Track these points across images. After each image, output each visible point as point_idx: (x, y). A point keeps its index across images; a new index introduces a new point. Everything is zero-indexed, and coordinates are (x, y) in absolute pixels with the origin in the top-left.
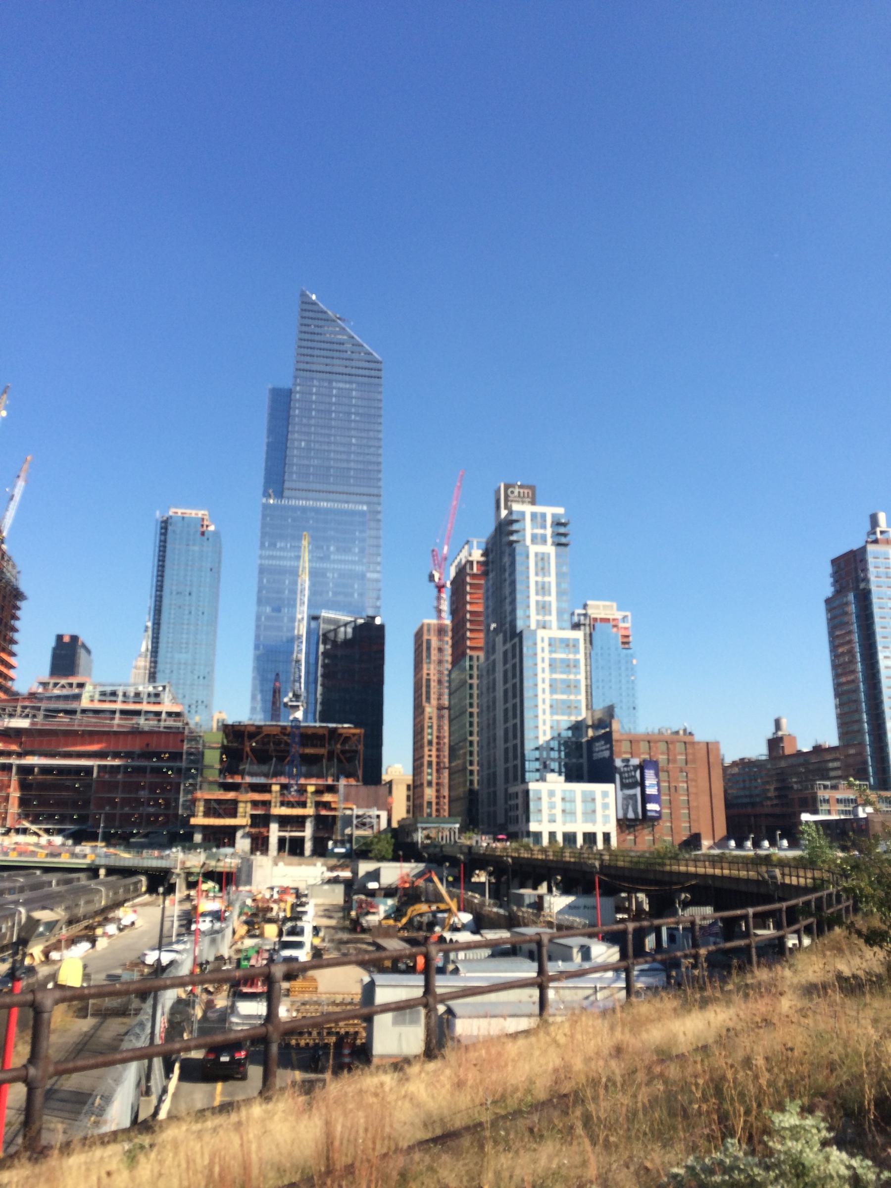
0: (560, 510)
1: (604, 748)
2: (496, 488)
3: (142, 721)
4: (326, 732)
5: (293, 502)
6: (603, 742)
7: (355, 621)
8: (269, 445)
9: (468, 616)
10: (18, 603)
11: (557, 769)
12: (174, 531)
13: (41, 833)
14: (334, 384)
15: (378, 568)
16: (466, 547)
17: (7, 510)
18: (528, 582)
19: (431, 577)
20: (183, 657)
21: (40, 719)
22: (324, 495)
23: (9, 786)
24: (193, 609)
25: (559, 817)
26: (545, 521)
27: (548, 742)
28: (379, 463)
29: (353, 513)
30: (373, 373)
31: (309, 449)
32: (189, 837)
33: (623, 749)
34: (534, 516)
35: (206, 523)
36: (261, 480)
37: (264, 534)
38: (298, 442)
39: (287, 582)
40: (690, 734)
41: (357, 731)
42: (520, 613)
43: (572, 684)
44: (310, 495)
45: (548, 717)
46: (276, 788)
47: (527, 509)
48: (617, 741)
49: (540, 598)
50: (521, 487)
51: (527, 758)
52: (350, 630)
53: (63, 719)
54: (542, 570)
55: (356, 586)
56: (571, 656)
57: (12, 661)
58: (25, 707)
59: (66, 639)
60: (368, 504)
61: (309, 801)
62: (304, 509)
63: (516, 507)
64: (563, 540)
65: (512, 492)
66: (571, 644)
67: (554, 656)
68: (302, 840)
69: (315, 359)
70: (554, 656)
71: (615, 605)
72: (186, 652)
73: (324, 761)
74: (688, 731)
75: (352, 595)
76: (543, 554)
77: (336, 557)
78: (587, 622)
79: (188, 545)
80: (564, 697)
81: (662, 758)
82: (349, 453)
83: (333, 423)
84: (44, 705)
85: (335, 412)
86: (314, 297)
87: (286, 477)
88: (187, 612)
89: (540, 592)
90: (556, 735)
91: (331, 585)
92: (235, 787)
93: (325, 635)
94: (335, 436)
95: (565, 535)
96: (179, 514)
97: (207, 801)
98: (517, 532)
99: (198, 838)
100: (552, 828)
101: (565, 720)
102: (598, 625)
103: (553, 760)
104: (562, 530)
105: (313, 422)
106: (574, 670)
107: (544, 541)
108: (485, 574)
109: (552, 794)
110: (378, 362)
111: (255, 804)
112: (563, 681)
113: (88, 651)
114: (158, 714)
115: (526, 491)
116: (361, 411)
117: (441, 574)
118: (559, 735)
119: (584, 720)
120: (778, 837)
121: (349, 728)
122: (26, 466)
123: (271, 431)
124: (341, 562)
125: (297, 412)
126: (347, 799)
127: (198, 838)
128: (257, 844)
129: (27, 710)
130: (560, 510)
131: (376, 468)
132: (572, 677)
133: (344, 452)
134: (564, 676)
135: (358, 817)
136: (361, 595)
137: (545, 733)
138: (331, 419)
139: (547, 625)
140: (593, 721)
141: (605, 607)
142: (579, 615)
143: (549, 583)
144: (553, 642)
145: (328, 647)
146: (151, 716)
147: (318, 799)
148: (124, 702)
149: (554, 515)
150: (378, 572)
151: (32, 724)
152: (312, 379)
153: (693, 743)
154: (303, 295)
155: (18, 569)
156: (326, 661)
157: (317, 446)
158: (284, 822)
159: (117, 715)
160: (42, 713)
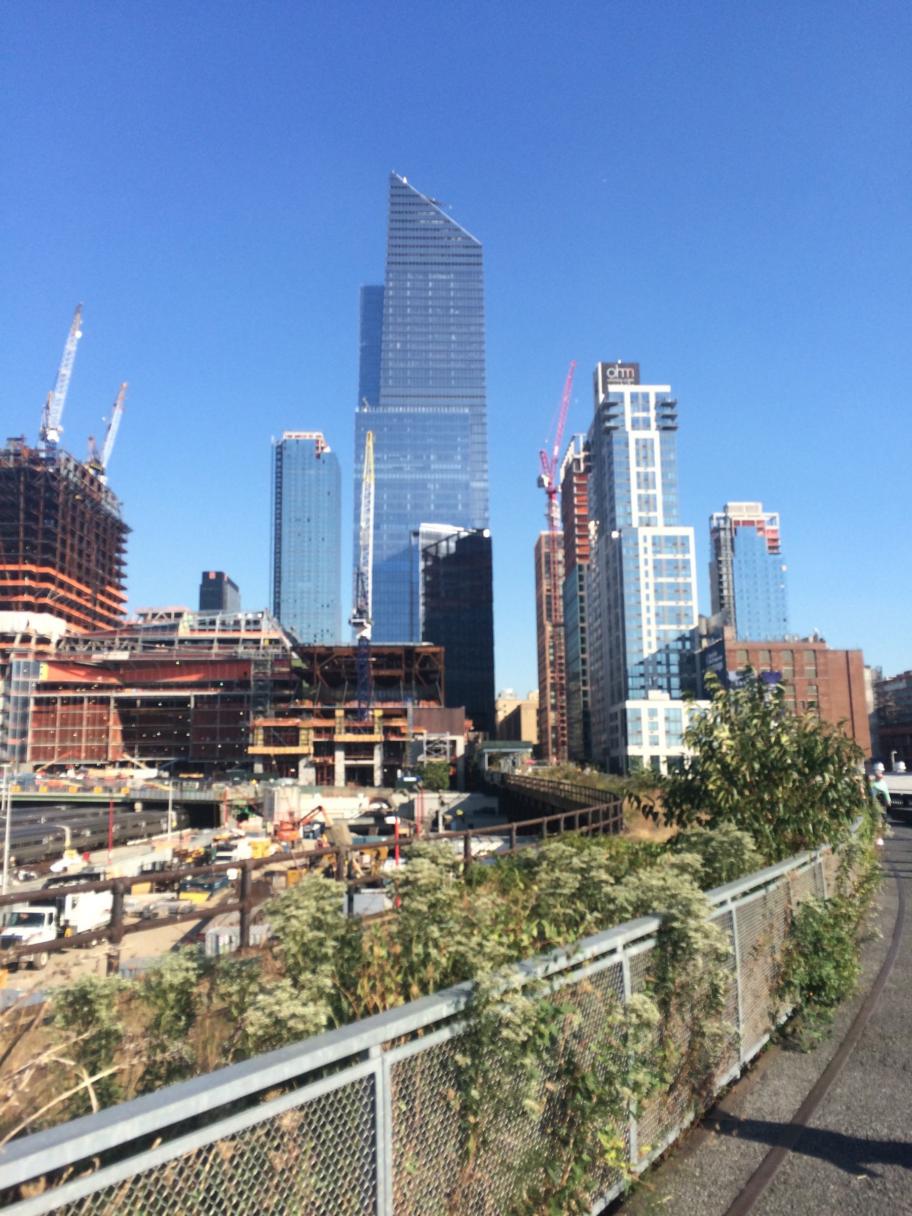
0: (666, 389)
1: (716, 659)
2: (593, 370)
3: (240, 649)
4: (402, 652)
5: (391, 410)
6: (715, 654)
7: (458, 534)
8: (363, 350)
9: (576, 521)
10: (124, 536)
11: (665, 685)
12: (289, 456)
13: (142, 765)
14: (430, 276)
15: (485, 477)
16: (572, 444)
17: (105, 440)
18: (628, 474)
19: (540, 482)
20: (306, 585)
21: (138, 651)
22: (423, 400)
23: (108, 720)
24: (313, 536)
25: (663, 739)
26: (648, 402)
27: (654, 656)
28: (482, 361)
29: (452, 417)
30: (472, 260)
31: (404, 351)
32: (249, 766)
33: (738, 660)
34: (634, 397)
35: (320, 445)
36: (357, 389)
38: (393, 343)
39: (385, 496)
40: (822, 641)
41: (437, 649)
42: (619, 510)
43: (682, 589)
44: (409, 400)
45: (653, 627)
46: (339, 713)
47: (627, 390)
48: (730, 651)
49: (642, 492)
50: (621, 366)
51: (630, 674)
52: (452, 545)
53: (162, 650)
54: (645, 457)
55: (460, 497)
56: (680, 557)
57: (122, 594)
58: (122, 640)
59: (212, 576)
60: (471, 406)
61: (376, 726)
62: (400, 417)
63: (612, 388)
64: (669, 423)
65: (612, 373)
66: (679, 542)
67: (659, 556)
68: (371, 768)
69: (408, 250)
70: (659, 556)
71: (760, 505)
72: (309, 580)
73: (401, 684)
74: (820, 637)
75: (456, 506)
76: (646, 440)
78: (728, 526)
79: (304, 469)
80: (672, 603)
81: (786, 670)
82: (448, 352)
83: (431, 320)
84: (141, 637)
86: (405, 181)
87: (382, 381)
88: (306, 539)
89: (643, 484)
90: (663, 647)
91: (432, 497)
92: (296, 713)
93: (425, 551)
94: (432, 333)
95: (672, 417)
97: (266, 729)
98: (614, 417)
99: (259, 768)
100: (655, 751)
101: (673, 630)
102: (740, 528)
103: (661, 675)
104: (668, 411)
105: (408, 320)
106: (683, 572)
107: (647, 426)
108: (588, 469)
109: (653, 713)
110: (479, 247)
111: (318, 731)
112: (670, 585)
113: (236, 588)
114: (257, 641)
115: (628, 370)
116: (460, 303)
117: (551, 478)
118: (667, 647)
119: (697, 628)
120: (893, 759)
122: (122, 394)
123: (365, 334)
124: (442, 471)
125: (391, 310)
126: (417, 723)
127: (259, 768)
128: (322, 774)
129: (125, 643)
130: (666, 389)
131: (478, 366)
132: (681, 580)
134: (671, 580)
135: (428, 742)
136: (466, 506)
137: (650, 646)
138: (428, 315)
139: (652, 522)
140: (708, 630)
141: (748, 508)
142: (718, 519)
143: (654, 473)
144: (657, 541)
145: (429, 563)
146: (250, 644)
147: (386, 724)
148: (224, 631)
149: (658, 395)
150: (485, 481)
151: (131, 656)
152: (405, 273)
153: (825, 652)
154: (393, 178)
155: (120, 500)
156: (428, 579)
158: (351, 749)
159: (216, 644)
160: (140, 644)
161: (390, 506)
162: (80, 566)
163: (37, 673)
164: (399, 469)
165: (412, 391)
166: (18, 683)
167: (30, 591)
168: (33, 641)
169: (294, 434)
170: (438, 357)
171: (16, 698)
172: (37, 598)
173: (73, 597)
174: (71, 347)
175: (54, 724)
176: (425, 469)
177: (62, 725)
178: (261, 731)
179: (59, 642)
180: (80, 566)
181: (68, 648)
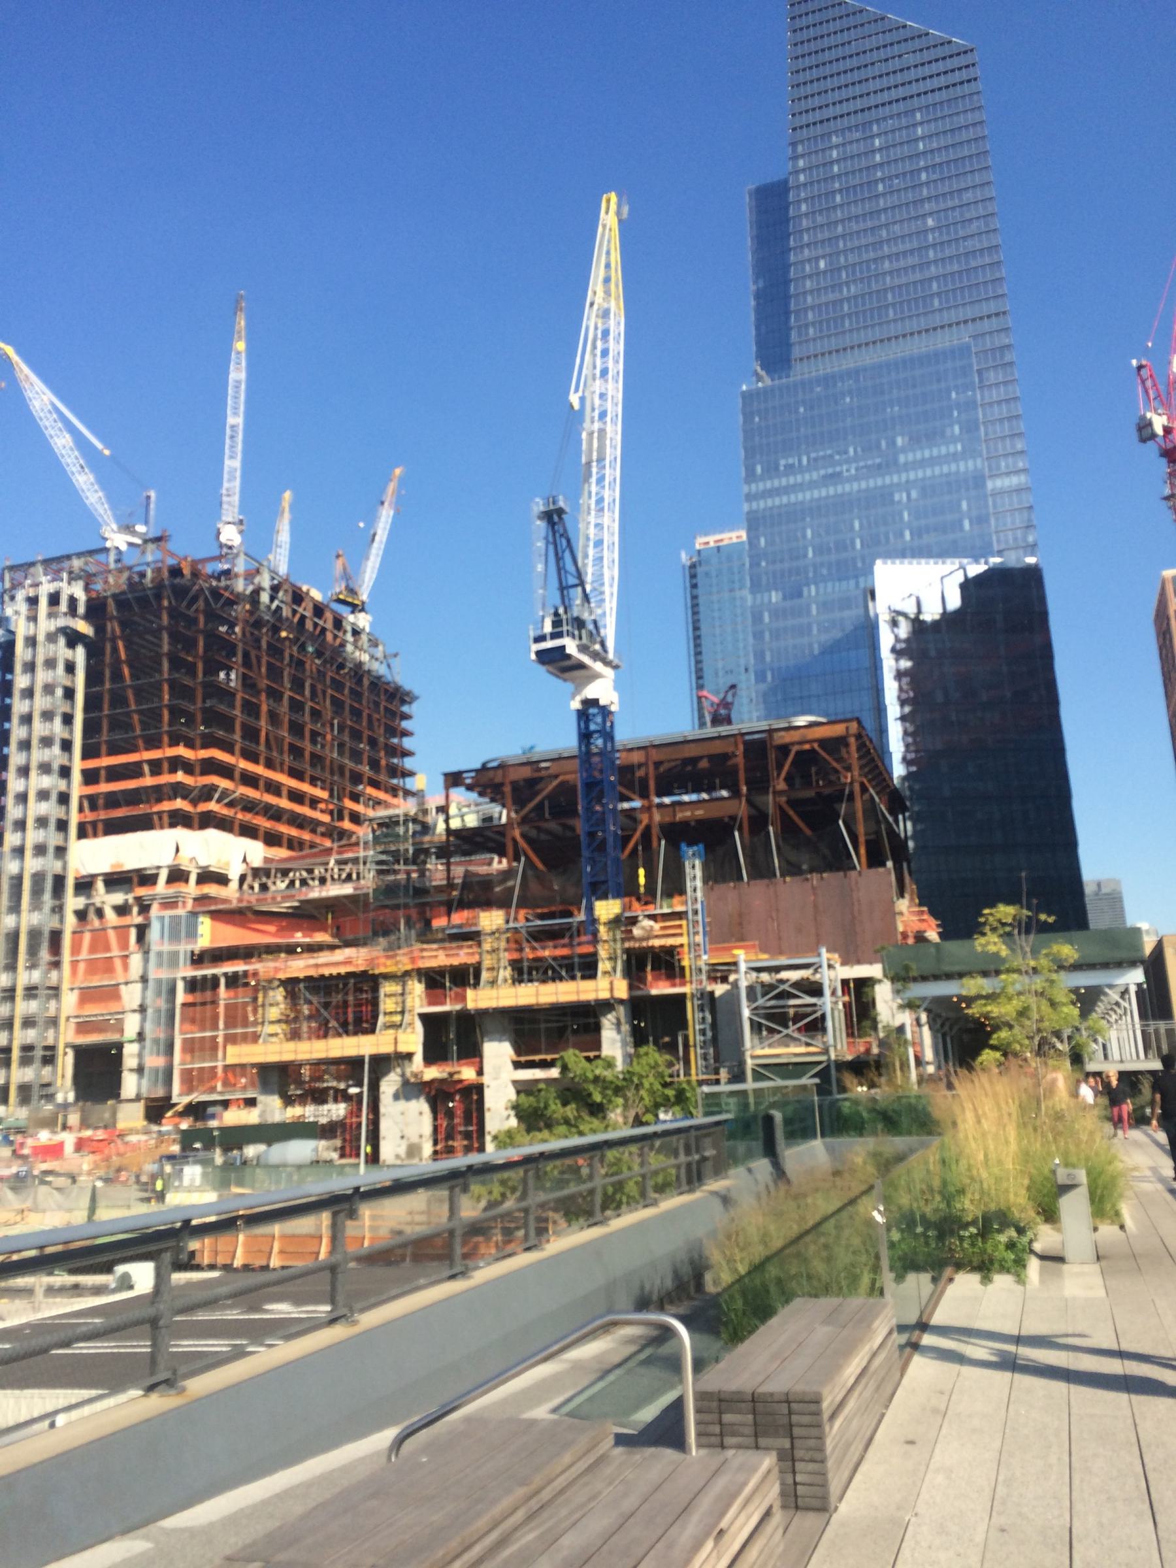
8: (758, 296)
10: (405, 709)
12: (707, 574)
29: (937, 357)
31: (834, 270)
37: (751, 452)
55: (964, 505)
62: (828, 381)
77: (910, 457)
79: (731, 590)
85: (882, 180)
87: (794, 336)
96: (712, 544)
111: (434, 980)
121: (812, 725)
122: (391, 487)
124: (923, 464)
133: (912, 251)
157: (852, 258)
161: (819, 550)
162: (296, 752)
163: (192, 934)
164: (835, 478)
165: (857, 338)
166: (160, 954)
167: (178, 790)
168: (193, 878)
169: (711, 540)
170: (902, 263)
171: (159, 982)
172: (194, 803)
173: (284, 803)
174: (238, 374)
175: (215, 1027)
176: (890, 465)
177: (227, 1027)
178: (279, 995)
179: (243, 878)
180: (296, 752)
181: (256, 886)
